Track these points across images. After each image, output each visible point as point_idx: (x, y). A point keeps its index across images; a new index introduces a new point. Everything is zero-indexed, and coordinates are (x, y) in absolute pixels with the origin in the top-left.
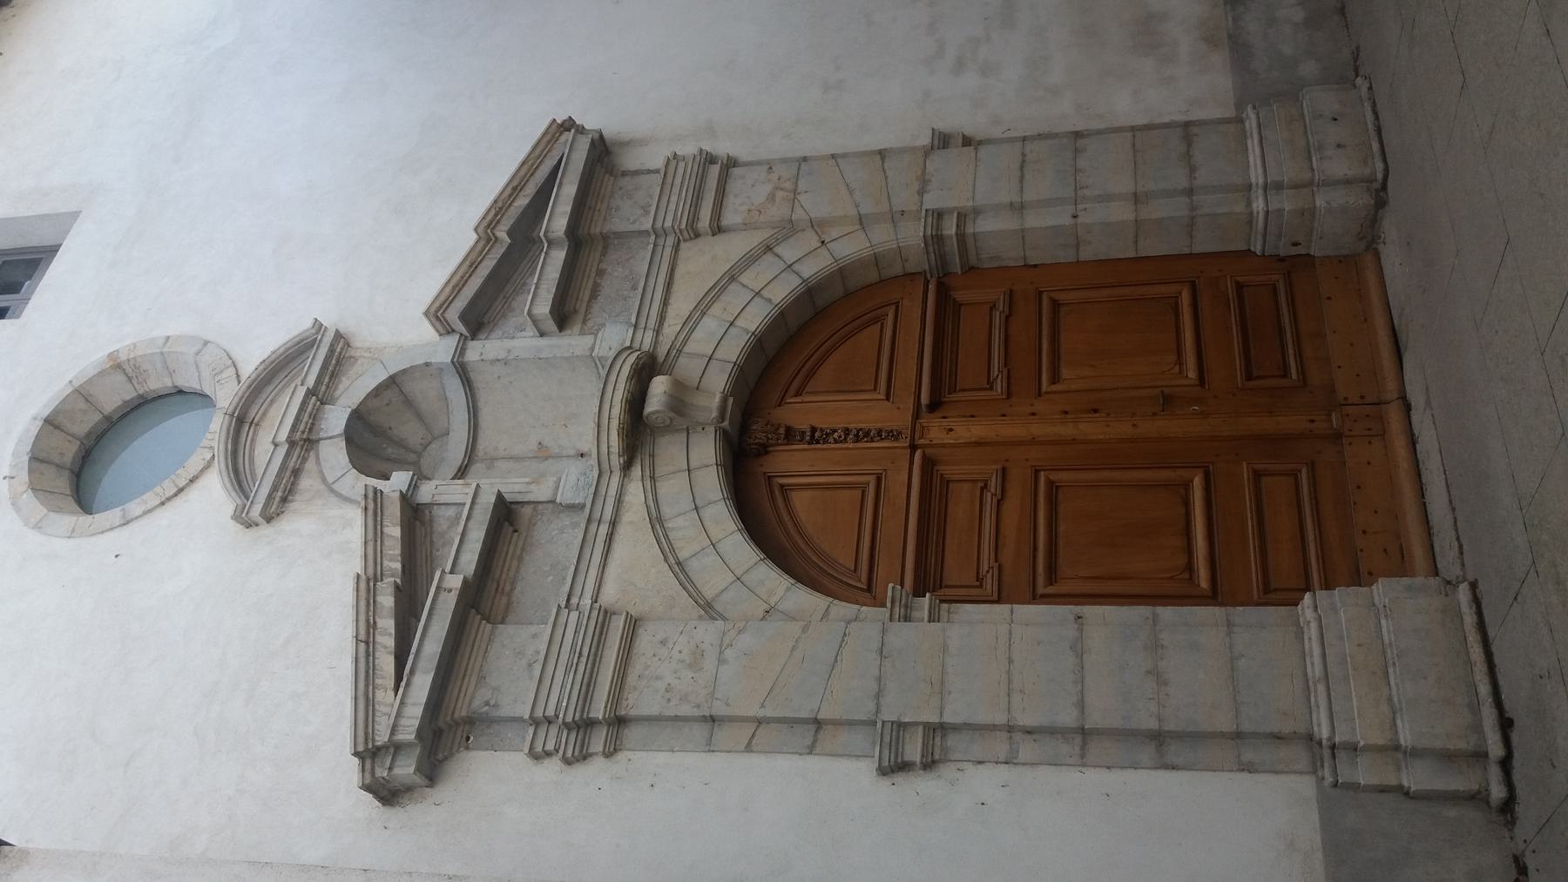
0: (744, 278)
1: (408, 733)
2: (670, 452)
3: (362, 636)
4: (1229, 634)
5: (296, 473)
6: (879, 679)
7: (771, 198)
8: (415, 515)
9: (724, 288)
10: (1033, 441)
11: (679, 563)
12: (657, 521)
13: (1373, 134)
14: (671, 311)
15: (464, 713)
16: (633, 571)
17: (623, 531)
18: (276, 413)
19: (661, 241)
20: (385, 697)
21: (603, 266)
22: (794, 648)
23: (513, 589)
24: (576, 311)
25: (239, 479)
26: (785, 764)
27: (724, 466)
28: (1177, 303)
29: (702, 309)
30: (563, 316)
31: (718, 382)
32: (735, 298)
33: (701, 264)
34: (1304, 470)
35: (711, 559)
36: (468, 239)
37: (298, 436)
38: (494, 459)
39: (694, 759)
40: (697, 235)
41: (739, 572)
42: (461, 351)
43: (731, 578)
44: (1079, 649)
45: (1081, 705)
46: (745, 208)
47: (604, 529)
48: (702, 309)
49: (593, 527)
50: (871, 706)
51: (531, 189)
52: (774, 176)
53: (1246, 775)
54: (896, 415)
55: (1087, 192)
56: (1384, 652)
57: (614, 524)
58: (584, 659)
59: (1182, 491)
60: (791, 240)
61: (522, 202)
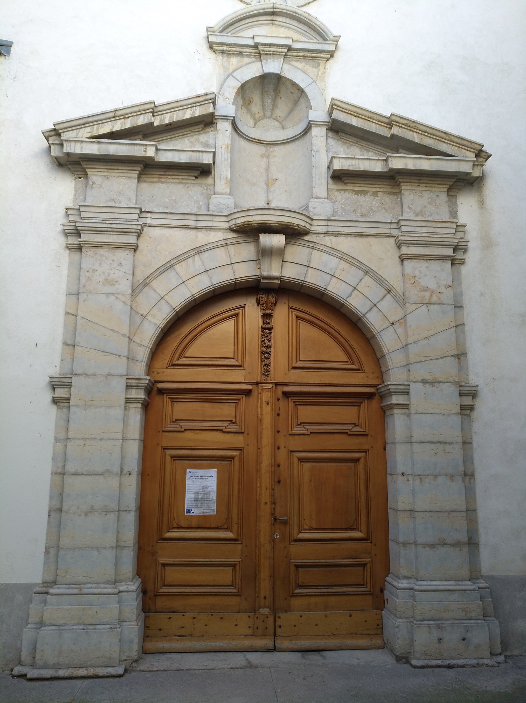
0: (367, 279)
1: (69, 148)
2: (247, 250)
3: (118, 113)
4: (112, 548)
5: (240, 54)
6: (94, 375)
7: (425, 289)
8: (207, 122)
9: (359, 268)
10: (259, 449)
11: (172, 266)
12: (199, 251)
13: (447, 662)
14: (341, 239)
15: (89, 173)
16: (164, 242)
17: (193, 232)
18: (282, 32)
19: (394, 226)
20: (86, 132)
21: (380, 194)
22: (113, 331)
23: (162, 183)
24: (345, 184)
25: (230, 25)
26: (59, 331)
27: (236, 283)
28: (354, 529)
29: (343, 257)
30: (339, 177)
31: (291, 273)
32: (352, 275)
33: (380, 254)
34: (234, 590)
35: (175, 282)
36: (386, 111)
37: (261, 48)
38: (268, 157)
39: (63, 287)
40: (399, 247)
41: (166, 298)
42: (319, 124)
43: (162, 294)
44: (106, 474)
45: (76, 474)
46: (417, 273)
47: (192, 223)
48: (343, 257)
49: (193, 217)
50: (80, 372)
51: (428, 142)
52: (443, 289)
53: (43, 550)
54: (281, 371)
55: (418, 481)
56: (92, 625)
57: (196, 228)
58: (109, 226)
59: (226, 526)
60: (396, 305)
61: (416, 138)
